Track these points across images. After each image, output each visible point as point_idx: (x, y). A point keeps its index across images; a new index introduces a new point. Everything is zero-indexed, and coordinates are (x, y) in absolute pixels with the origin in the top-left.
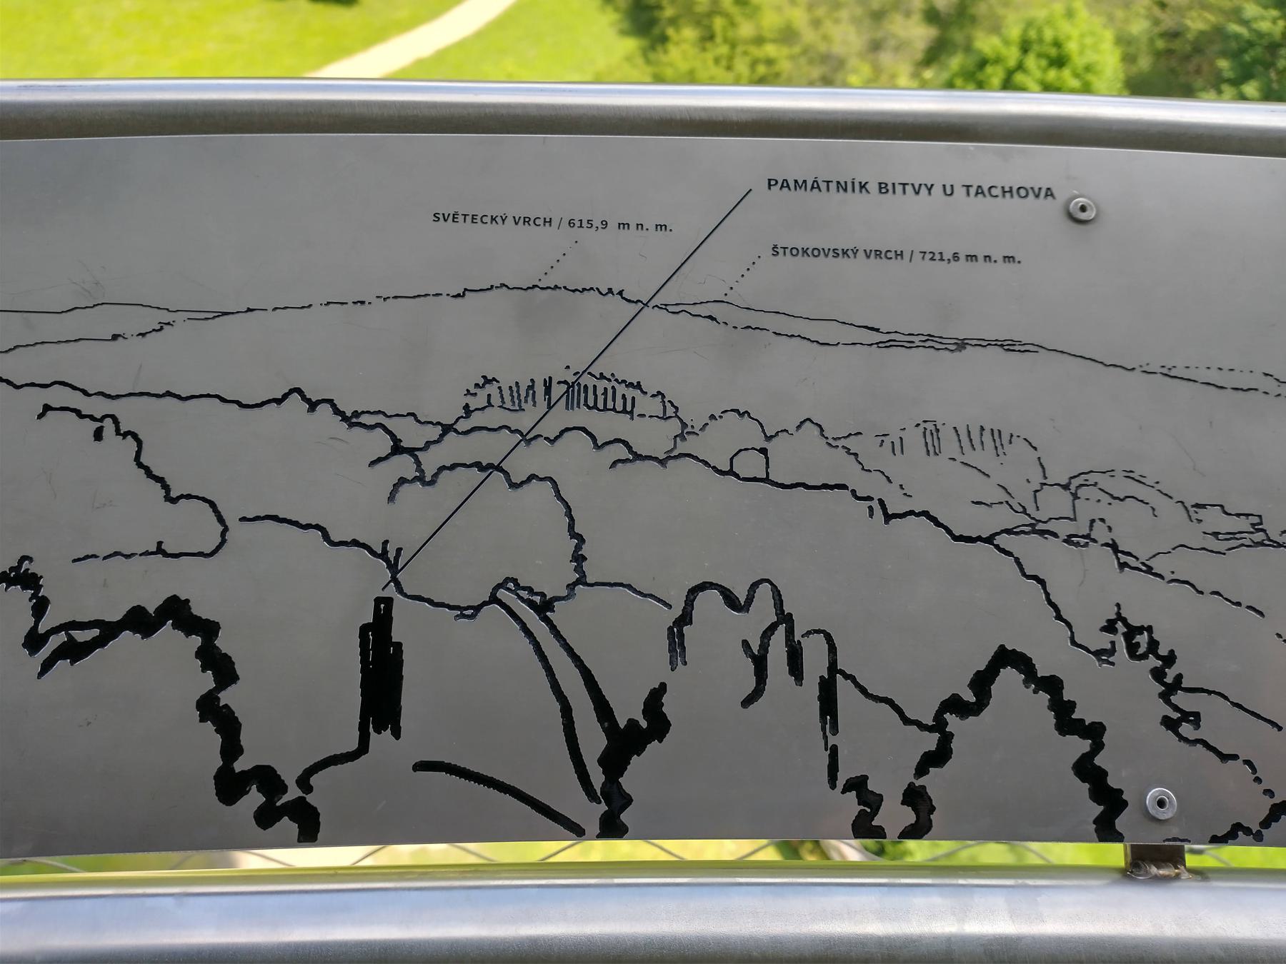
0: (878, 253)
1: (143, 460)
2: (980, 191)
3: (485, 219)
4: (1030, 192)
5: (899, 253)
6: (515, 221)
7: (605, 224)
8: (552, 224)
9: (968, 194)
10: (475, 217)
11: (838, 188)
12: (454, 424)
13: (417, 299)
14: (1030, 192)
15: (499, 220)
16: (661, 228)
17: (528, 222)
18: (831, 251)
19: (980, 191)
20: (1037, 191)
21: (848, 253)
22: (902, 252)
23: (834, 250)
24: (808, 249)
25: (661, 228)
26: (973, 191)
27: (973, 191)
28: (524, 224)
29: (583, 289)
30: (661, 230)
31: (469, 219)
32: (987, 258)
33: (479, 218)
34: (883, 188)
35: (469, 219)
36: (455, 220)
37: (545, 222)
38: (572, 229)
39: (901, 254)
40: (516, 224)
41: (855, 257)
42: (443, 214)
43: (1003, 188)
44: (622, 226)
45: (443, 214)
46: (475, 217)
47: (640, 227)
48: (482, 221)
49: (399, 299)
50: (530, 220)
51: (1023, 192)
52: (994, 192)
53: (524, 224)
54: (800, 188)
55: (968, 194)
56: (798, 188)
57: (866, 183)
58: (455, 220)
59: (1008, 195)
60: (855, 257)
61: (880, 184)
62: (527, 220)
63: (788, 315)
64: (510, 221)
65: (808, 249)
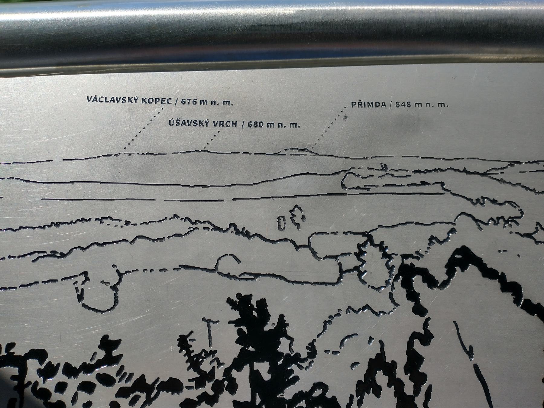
0: (222, 123)
1: (139, 240)
3: (228, 124)
5: (234, 123)
6: (88, 99)
7: (409, 103)
11: (479, 225)
12: (533, 234)
15: (133, 100)
16: (418, 105)
17: (361, 105)
18: (193, 122)
21: (132, 100)
22: (236, 122)
24: (146, 98)
25: (418, 105)
28: (359, 107)
29: (102, 218)
30: (441, 107)
32: (213, 102)
33: (166, 100)
37: (233, 124)
38: (195, 105)
39: (236, 124)
40: (89, 101)
41: (136, 102)
42: (188, 121)
44: (417, 105)
45: (188, 121)
47: (428, 105)
48: (168, 102)
49: (320, 235)
53: (359, 107)
60: (136, 102)
63: (392, 226)
64: (211, 124)
65: (146, 98)
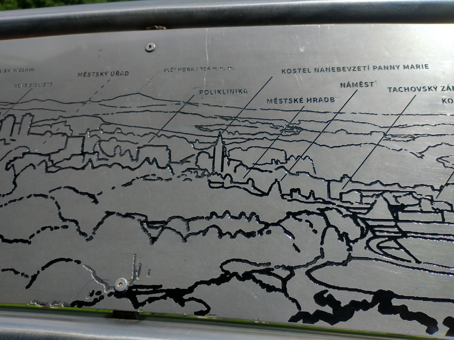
2: (395, 89)
3: (21, 70)
4: (416, 89)
8: (307, 99)
9: (390, 91)
10: (426, 66)
13: (71, 104)
14: (416, 89)
19: (395, 89)
20: (419, 88)
23: (290, 99)
26: (392, 90)
27: (392, 90)
31: (301, 71)
34: (374, 68)
35: (301, 71)
36: (301, 101)
43: (405, 88)
46: (426, 66)
50: (317, 100)
51: (413, 89)
52: (401, 89)
54: (80, 75)
55: (390, 91)
56: (79, 76)
57: (241, 89)
58: (301, 101)
59: (407, 90)
61: (338, 68)
62: (315, 99)
